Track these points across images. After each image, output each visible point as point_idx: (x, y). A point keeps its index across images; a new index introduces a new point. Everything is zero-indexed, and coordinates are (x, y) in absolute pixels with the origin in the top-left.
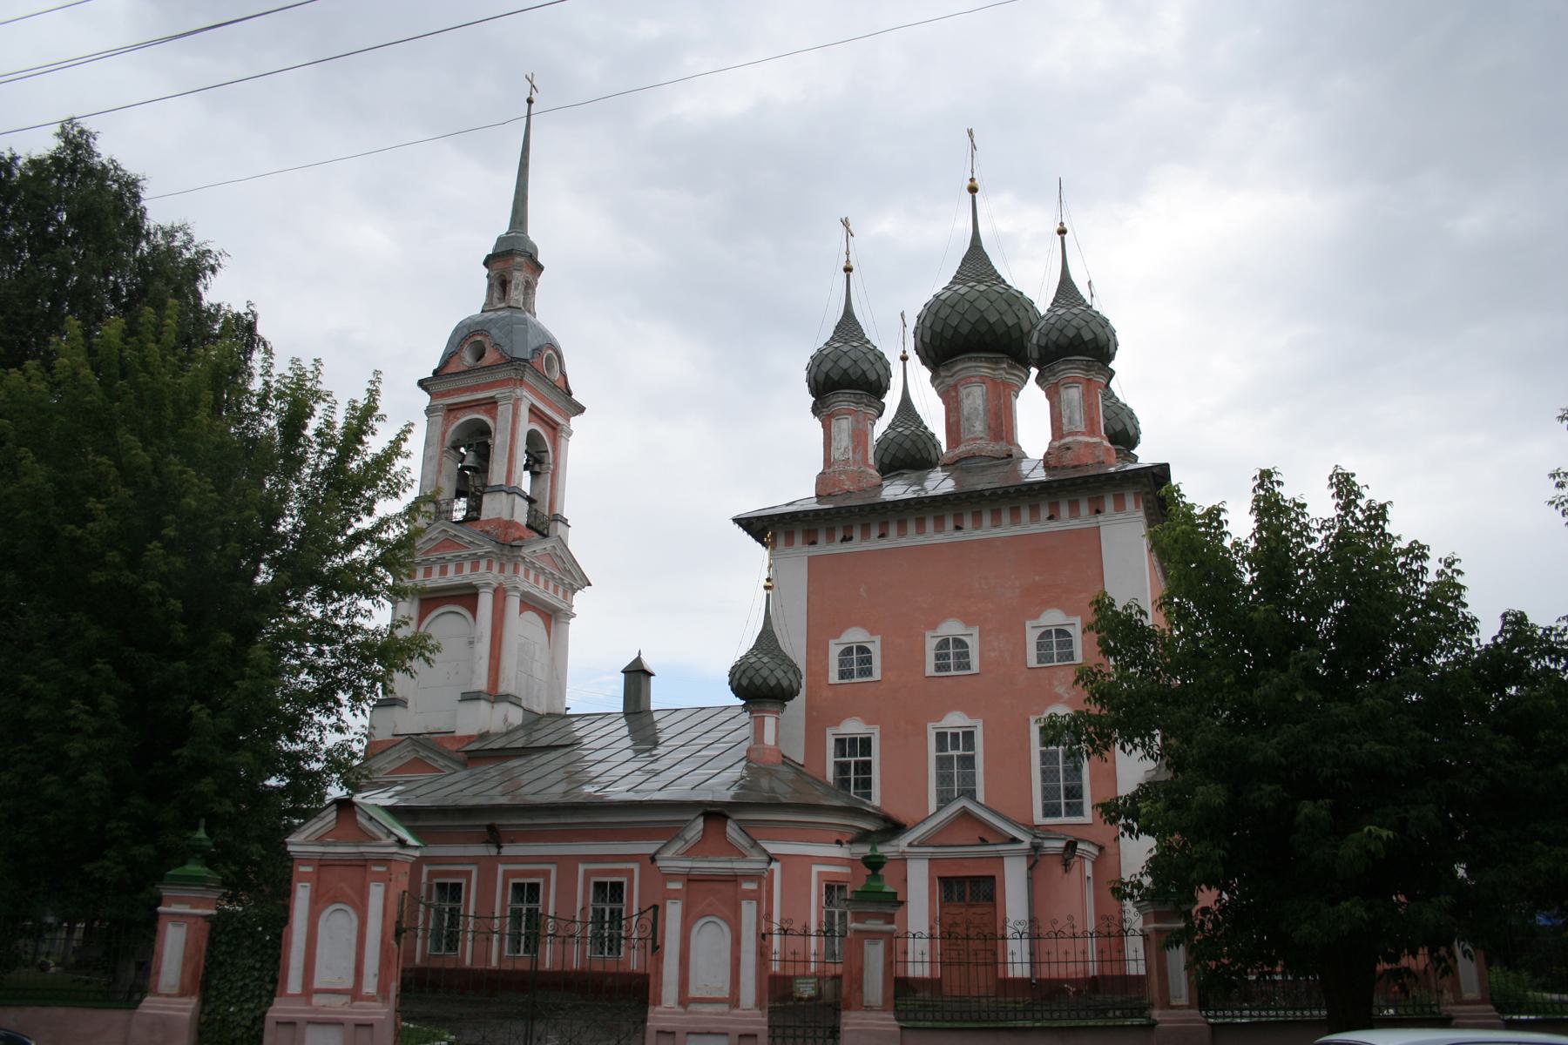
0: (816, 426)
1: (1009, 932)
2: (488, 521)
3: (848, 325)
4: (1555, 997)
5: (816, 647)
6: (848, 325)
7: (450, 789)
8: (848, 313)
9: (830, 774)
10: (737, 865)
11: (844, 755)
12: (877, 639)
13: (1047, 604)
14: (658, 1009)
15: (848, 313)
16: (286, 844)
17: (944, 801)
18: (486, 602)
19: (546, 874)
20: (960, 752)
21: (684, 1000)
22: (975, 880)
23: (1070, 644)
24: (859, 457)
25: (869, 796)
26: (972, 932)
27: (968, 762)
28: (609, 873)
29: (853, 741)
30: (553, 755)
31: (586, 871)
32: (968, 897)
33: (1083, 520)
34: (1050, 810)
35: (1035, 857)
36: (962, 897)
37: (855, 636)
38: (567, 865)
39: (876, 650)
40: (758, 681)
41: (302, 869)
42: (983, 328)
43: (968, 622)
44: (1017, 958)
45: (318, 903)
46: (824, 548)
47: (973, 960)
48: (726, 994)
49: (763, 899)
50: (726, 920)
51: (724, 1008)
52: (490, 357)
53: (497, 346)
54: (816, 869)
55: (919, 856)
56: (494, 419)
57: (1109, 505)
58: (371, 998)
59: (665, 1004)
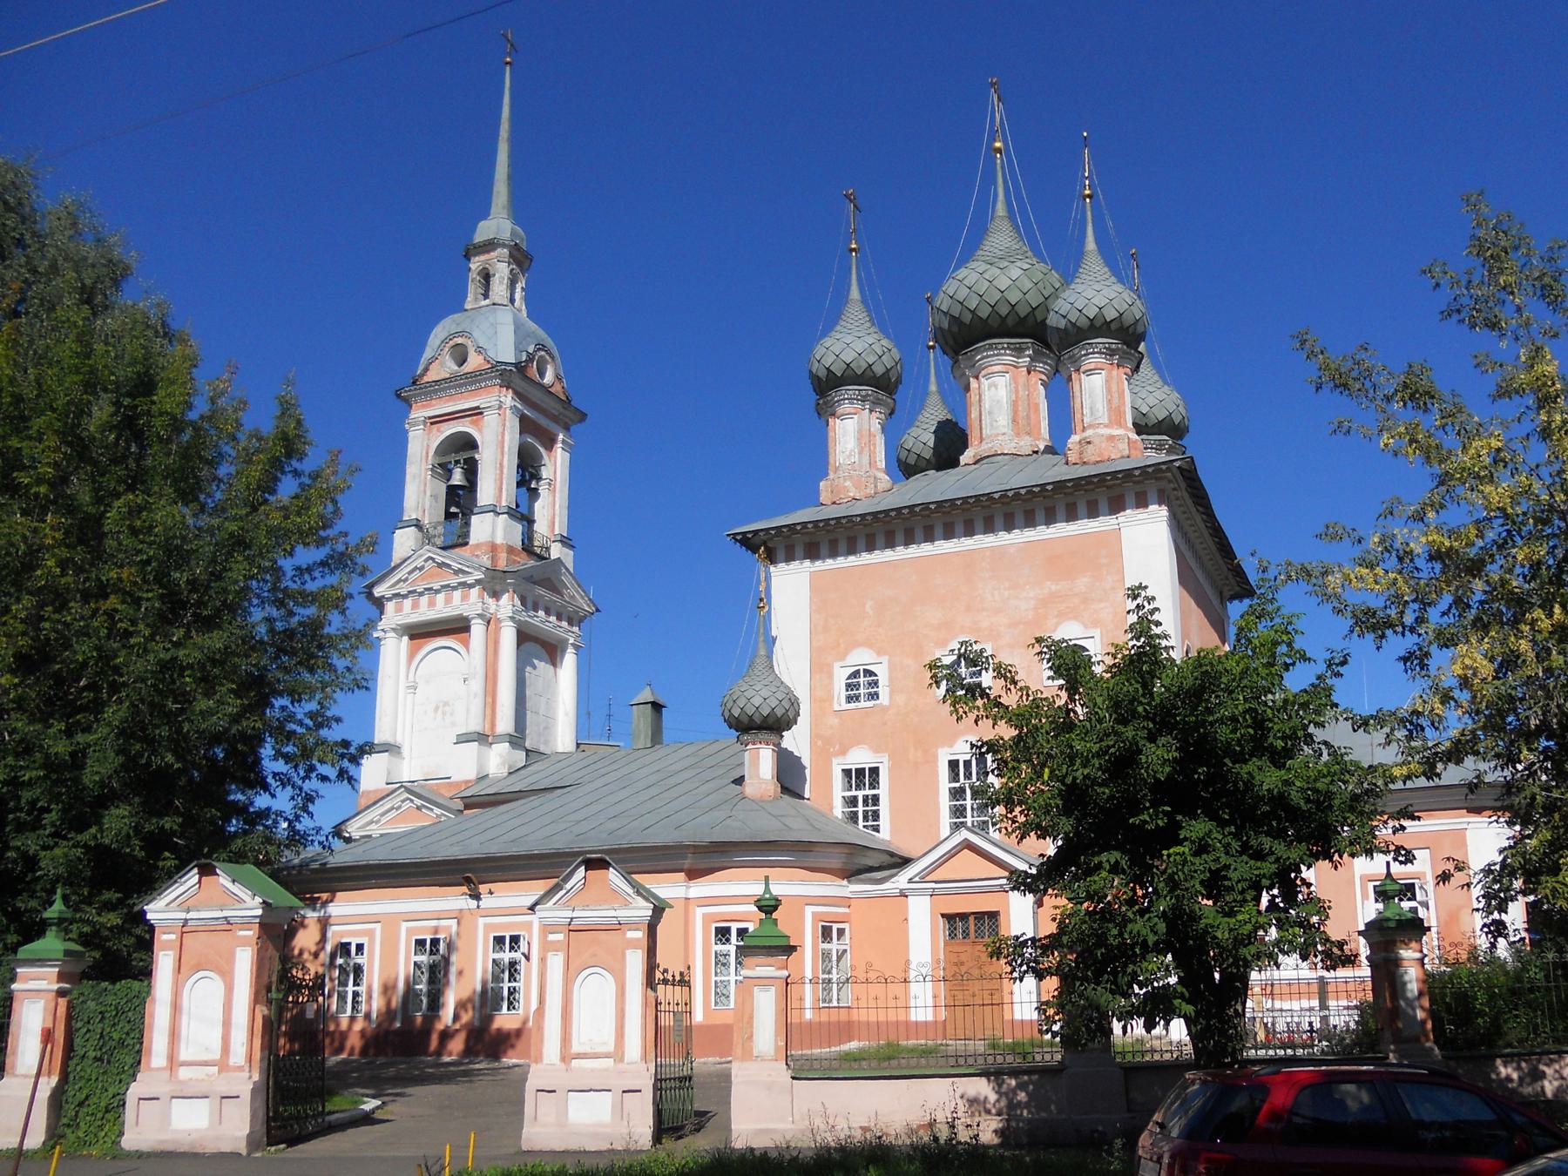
1: (912, 975)
2: (478, 546)
4: (817, 1051)
5: (819, 669)
7: (429, 840)
9: (839, 810)
12: (885, 659)
14: (540, 1066)
16: (144, 913)
18: (477, 629)
19: (371, 934)
21: (566, 1056)
22: (980, 916)
24: (866, 460)
29: (860, 772)
30: (549, 796)
31: (704, 915)
32: (972, 934)
36: (966, 934)
37: (861, 657)
38: (390, 922)
41: (165, 937)
44: (920, 1003)
48: (611, 1048)
51: (608, 1063)
52: (474, 362)
53: (480, 350)
54: (809, 910)
55: (919, 892)
56: (480, 431)
58: (240, 1069)
59: (546, 1060)
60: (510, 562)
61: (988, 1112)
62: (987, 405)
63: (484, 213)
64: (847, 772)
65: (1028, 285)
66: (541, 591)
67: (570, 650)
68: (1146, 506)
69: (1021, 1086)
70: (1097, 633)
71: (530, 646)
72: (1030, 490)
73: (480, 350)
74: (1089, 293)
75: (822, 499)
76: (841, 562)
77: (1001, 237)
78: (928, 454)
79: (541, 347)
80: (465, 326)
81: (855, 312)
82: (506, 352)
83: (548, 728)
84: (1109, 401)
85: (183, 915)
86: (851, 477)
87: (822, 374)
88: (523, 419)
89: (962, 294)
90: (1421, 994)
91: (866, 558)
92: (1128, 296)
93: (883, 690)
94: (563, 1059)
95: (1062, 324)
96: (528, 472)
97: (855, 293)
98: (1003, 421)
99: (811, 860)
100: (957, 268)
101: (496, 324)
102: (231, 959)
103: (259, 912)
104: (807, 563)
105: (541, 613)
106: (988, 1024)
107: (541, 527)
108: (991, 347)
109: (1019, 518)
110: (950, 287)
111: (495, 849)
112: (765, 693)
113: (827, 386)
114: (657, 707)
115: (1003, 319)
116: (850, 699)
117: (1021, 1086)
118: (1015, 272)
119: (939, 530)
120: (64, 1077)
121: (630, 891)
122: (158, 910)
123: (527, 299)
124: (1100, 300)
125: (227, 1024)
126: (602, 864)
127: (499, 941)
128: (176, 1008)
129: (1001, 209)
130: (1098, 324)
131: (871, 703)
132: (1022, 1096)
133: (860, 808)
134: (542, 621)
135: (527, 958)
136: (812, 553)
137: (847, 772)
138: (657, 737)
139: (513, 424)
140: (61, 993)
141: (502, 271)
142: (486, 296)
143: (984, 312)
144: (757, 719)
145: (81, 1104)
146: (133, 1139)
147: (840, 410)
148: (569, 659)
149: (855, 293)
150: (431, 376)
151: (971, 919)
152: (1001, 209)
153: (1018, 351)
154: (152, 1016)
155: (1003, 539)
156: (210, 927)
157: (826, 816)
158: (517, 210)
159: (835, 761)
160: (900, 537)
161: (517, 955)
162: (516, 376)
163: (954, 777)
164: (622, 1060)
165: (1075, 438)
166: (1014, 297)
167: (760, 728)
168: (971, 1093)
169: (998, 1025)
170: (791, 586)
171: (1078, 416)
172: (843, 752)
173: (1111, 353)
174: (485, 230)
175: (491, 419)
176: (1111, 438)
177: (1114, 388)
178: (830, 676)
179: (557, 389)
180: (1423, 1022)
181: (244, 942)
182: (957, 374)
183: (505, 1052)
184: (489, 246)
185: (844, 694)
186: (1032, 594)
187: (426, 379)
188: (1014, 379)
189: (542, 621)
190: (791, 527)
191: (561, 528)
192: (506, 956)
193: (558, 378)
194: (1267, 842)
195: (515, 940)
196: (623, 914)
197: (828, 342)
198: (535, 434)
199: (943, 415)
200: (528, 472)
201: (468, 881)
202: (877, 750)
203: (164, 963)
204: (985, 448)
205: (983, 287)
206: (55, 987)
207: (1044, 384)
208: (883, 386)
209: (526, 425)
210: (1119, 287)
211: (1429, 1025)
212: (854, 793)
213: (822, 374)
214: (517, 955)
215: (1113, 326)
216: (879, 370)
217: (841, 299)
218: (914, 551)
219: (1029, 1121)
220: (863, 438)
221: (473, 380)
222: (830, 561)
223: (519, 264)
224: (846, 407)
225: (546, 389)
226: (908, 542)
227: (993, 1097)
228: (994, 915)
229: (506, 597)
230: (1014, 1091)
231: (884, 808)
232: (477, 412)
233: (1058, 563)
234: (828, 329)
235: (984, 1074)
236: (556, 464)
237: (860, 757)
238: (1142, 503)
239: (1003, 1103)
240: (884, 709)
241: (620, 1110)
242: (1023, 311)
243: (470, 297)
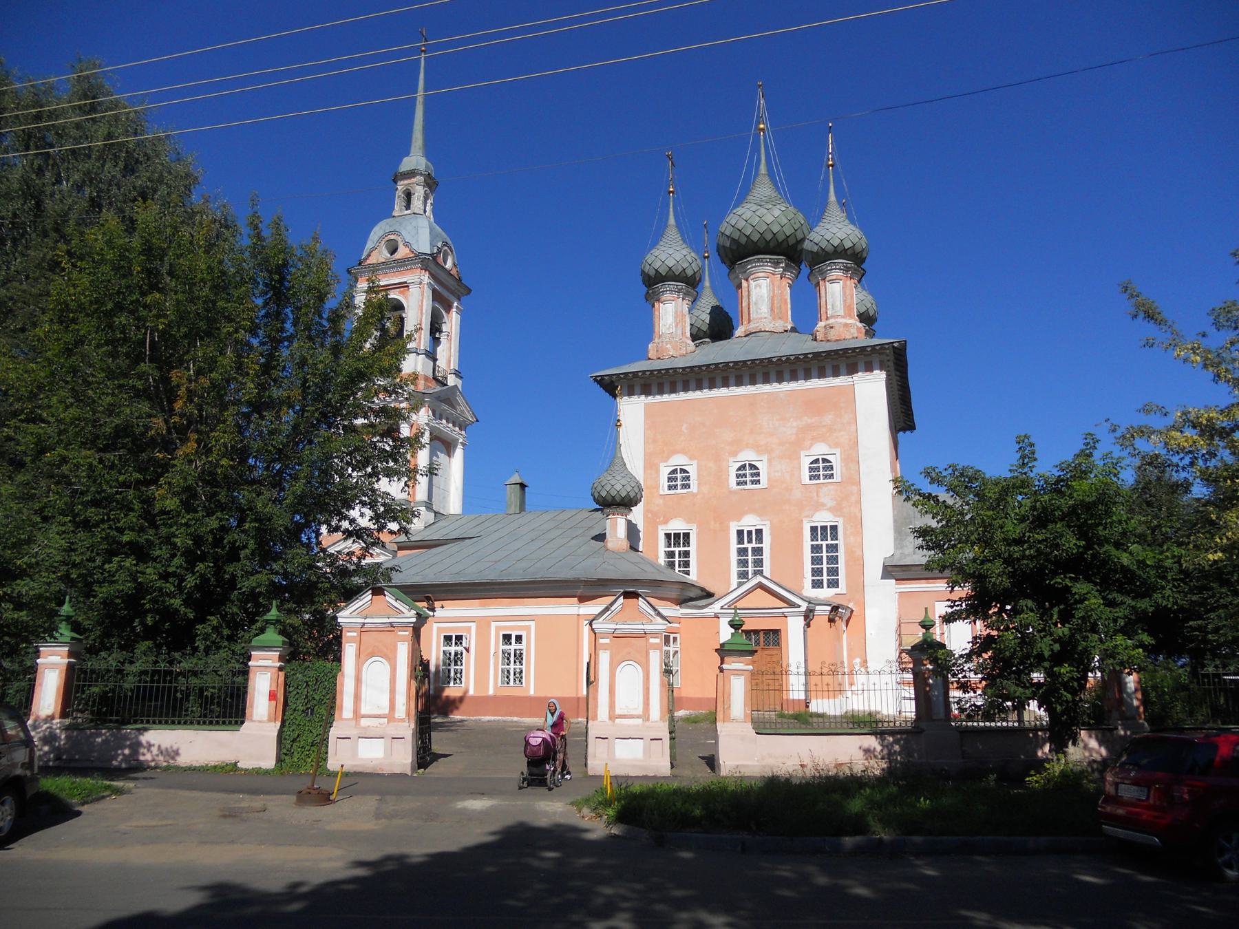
9: (662, 560)
10: (645, 627)
11: (669, 546)
13: (815, 440)
17: (743, 575)
20: (754, 545)
21: (613, 717)
22: (767, 632)
24: (679, 332)
25: (687, 573)
26: (825, 671)
28: (454, 629)
30: (462, 543)
34: (817, 584)
35: (808, 616)
37: (679, 460)
38: (483, 623)
39: (693, 472)
40: (614, 493)
42: (769, 237)
43: (759, 452)
45: (360, 659)
47: (872, 687)
48: (640, 711)
51: (640, 721)
52: (402, 252)
53: (406, 244)
54: (493, 625)
58: (403, 720)
60: (427, 387)
61: (875, 757)
62: (753, 299)
63: (407, 153)
64: (668, 536)
65: (784, 221)
66: (445, 407)
67: (460, 446)
68: (872, 371)
69: (896, 742)
70: (838, 451)
71: (437, 443)
72: (797, 357)
73: (406, 244)
74: (748, 215)
75: (650, 355)
76: (666, 398)
77: (763, 188)
78: (705, 328)
79: (446, 244)
80: (397, 227)
81: (672, 233)
82: (424, 246)
83: (445, 498)
84: (845, 301)
85: (363, 621)
86: (671, 342)
87: (652, 273)
88: (434, 292)
89: (741, 224)
90: (1136, 690)
91: (682, 396)
92: (858, 233)
93: (693, 482)
94: (610, 718)
95: (815, 249)
96: (436, 328)
97: (672, 221)
98: (764, 309)
99: (661, 593)
100: (735, 207)
101: (417, 228)
102: (394, 650)
103: (414, 620)
104: (643, 397)
105: (444, 421)
106: (772, 702)
107: (442, 363)
108: (759, 260)
109: (787, 375)
110: (732, 219)
111: (447, 578)
112: (623, 482)
113: (654, 282)
114: (523, 486)
115: (768, 243)
116: (670, 487)
117: (896, 742)
118: (777, 213)
119: (732, 380)
120: (283, 722)
121: (652, 613)
122: (348, 616)
123: (434, 211)
124: (841, 235)
125: (393, 691)
126: (635, 595)
127: (448, 639)
128: (358, 680)
129: (763, 168)
130: (839, 250)
131: (685, 491)
132: (897, 748)
133: (677, 559)
134: (445, 426)
135: (467, 650)
136: (646, 391)
137: (668, 536)
138: (522, 508)
139: (428, 294)
140: (280, 669)
141: (419, 191)
142: (408, 207)
143: (755, 237)
144: (618, 499)
145: (294, 740)
146: (333, 764)
147: (663, 298)
148: (459, 452)
149: (672, 221)
150: (373, 260)
151: (761, 634)
152: (763, 168)
153: (776, 264)
154: (342, 685)
155: (775, 388)
156: (379, 629)
157: (654, 566)
158: (429, 152)
159: (660, 528)
160: (706, 383)
161: (460, 648)
162: (430, 263)
163: (740, 541)
164: (648, 719)
165: (821, 324)
166: (775, 229)
167: (619, 505)
168: (866, 745)
169: (778, 703)
170: (632, 409)
171: (823, 310)
172: (666, 522)
173: (846, 269)
174: (407, 164)
175: (414, 291)
176: (846, 325)
177: (848, 292)
178: (658, 471)
179: (454, 272)
180: (1138, 707)
181: (403, 639)
182: (732, 276)
183: (452, 712)
184: (411, 174)
185: (666, 484)
186: (795, 424)
187: (368, 262)
188: (772, 282)
189: (445, 426)
190: (635, 374)
191: (454, 365)
192: (453, 649)
193: (455, 265)
194: (1119, 598)
195: (459, 638)
196: (648, 627)
197: (656, 252)
198: (441, 301)
199: (714, 302)
200: (436, 328)
201: (428, 599)
202: (689, 521)
203: (349, 652)
204: (753, 327)
205: (755, 221)
206: (278, 664)
207: (790, 286)
208: (690, 283)
209: (436, 296)
210: (851, 227)
211: (1141, 709)
212: (672, 549)
213: (652, 273)
214: (460, 648)
215: (849, 252)
216: (689, 273)
217: (664, 225)
218: (715, 393)
219: (901, 763)
220: (678, 316)
221: (403, 264)
222: (658, 397)
223: (430, 188)
224: (668, 296)
225: (448, 272)
226: (711, 387)
227: (879, 748)
228: (776, 632)
229: (423, 410)
230: (892, 744)
231: (693, 559)
232: (405, 286)
233: (813, 405)
234: (654, 244)
235: (874, 733)
236: (452, 322)
237: (677, 526)
238: (869, 368)
239: (885, 752)
240: (694, 495)
241: (389, 751)
242: (781, 238)
243: (397, 208)
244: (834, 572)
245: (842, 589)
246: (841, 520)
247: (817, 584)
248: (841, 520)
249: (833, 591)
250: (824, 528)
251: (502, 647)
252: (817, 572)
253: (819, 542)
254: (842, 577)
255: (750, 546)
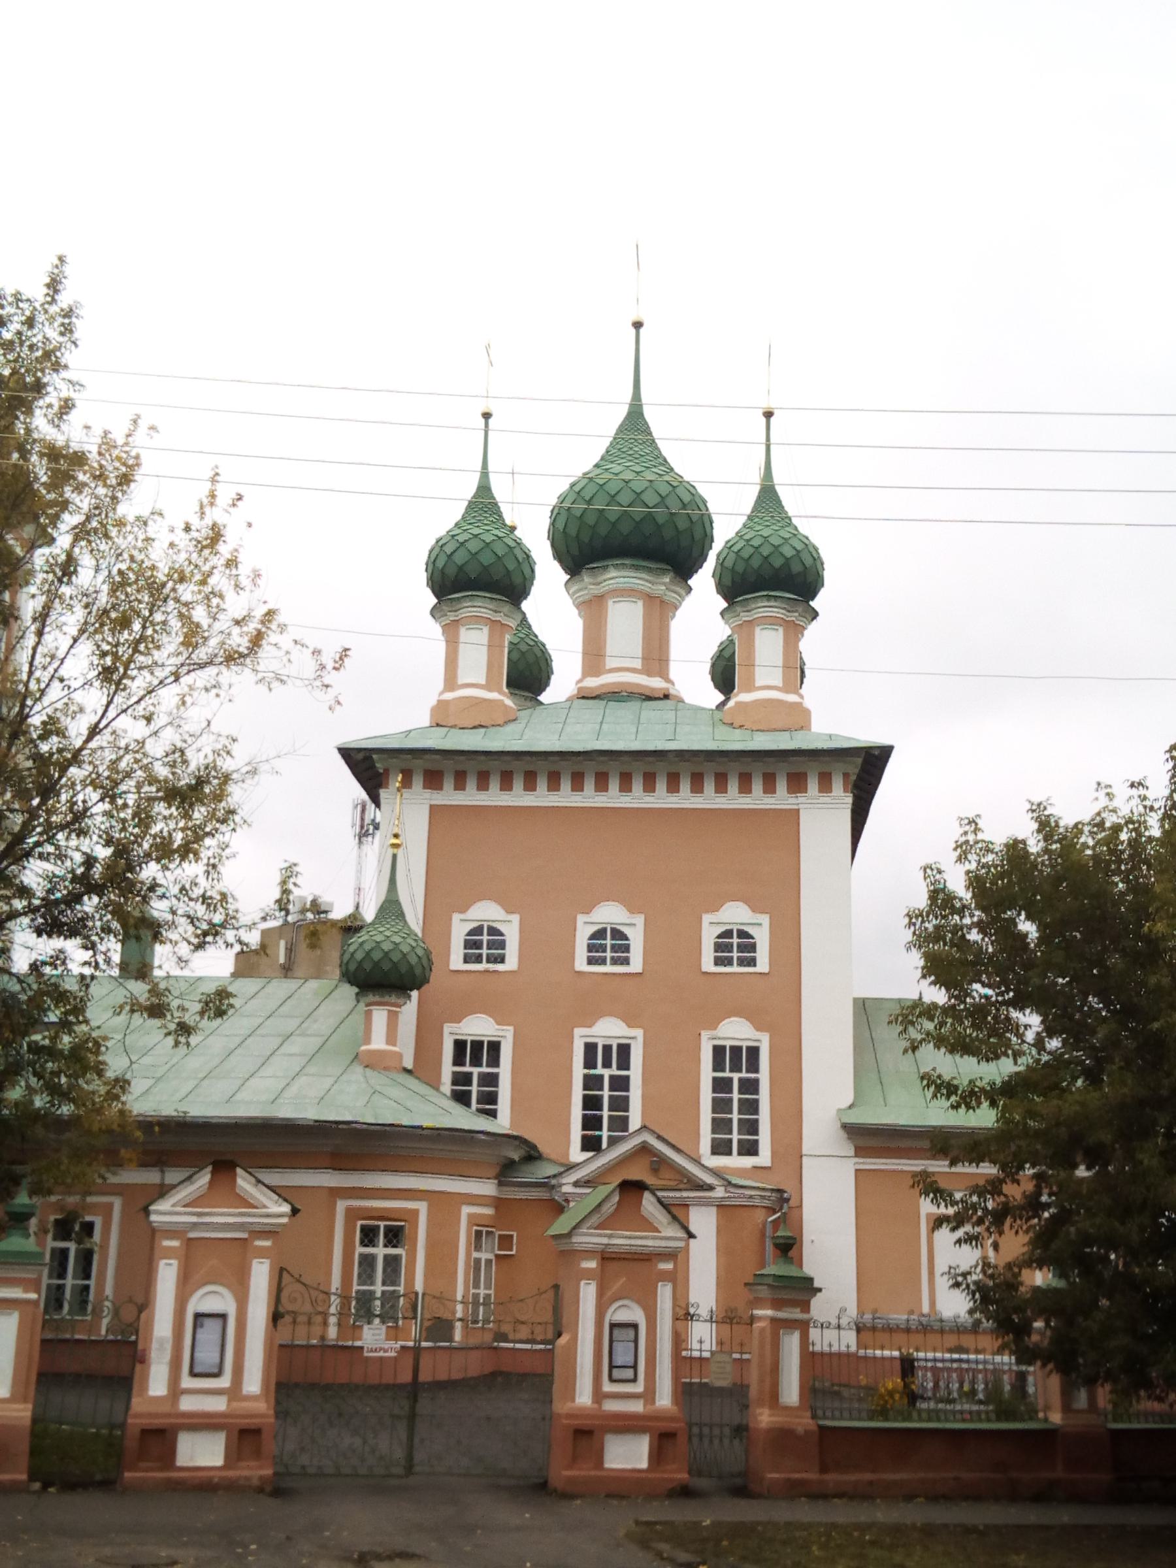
0: (435, 629)
3: (483, 503)
6: (483, 503)
8: (484, 489)
15: (484, 489)
23: (627, 949)
26: (844, 1322)
27: (620, 1084)
33: (781, 799)
34: (721, 1148)
41: (167, 1243)
46: (449, 796)
49: (679, 1279)
50: (638, 1302)
54: (466, 1210)
57: (813, 785)
108: (769, 597)
244: (751, 1127)
245: (764, 1157)
246: (639, 1033)
247: (721, 1148)
248: (639, 1033)
249: (748, 1162)
250: (736, 1050)
251: (360, 1250)
252: (721, 1125)
253: (727, 1074)
254: (764, 1137)
255: (606, 1073)
